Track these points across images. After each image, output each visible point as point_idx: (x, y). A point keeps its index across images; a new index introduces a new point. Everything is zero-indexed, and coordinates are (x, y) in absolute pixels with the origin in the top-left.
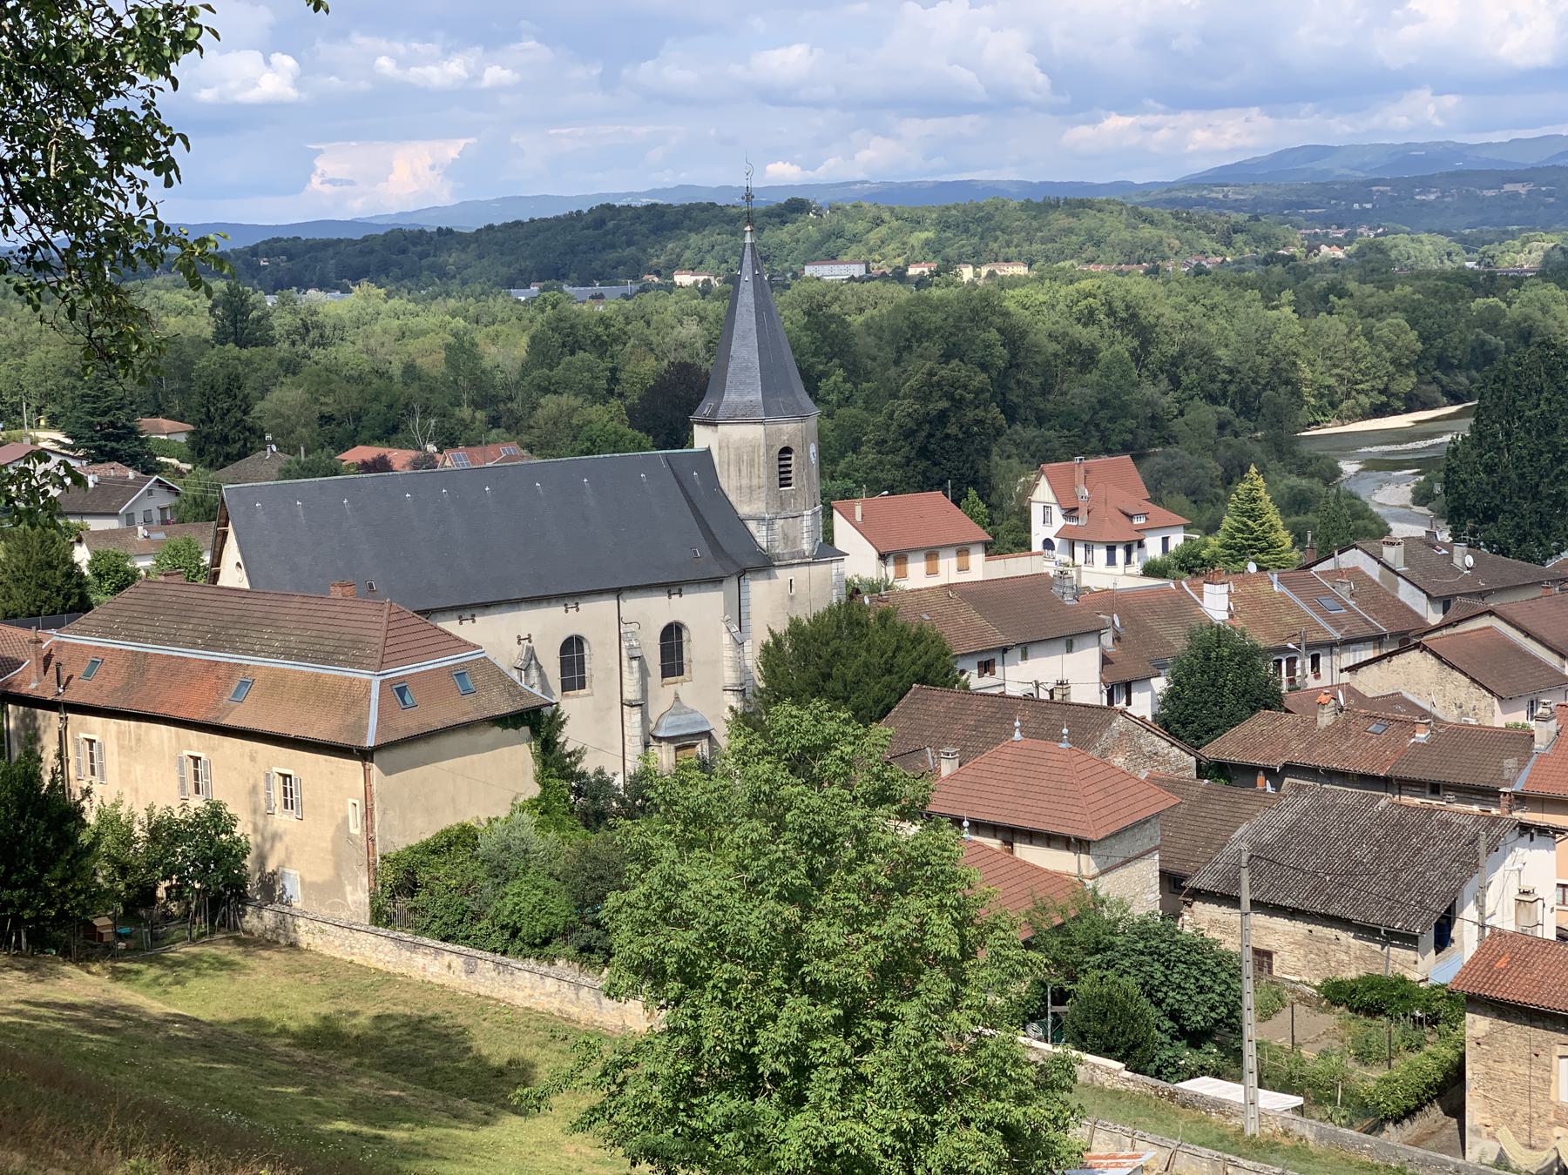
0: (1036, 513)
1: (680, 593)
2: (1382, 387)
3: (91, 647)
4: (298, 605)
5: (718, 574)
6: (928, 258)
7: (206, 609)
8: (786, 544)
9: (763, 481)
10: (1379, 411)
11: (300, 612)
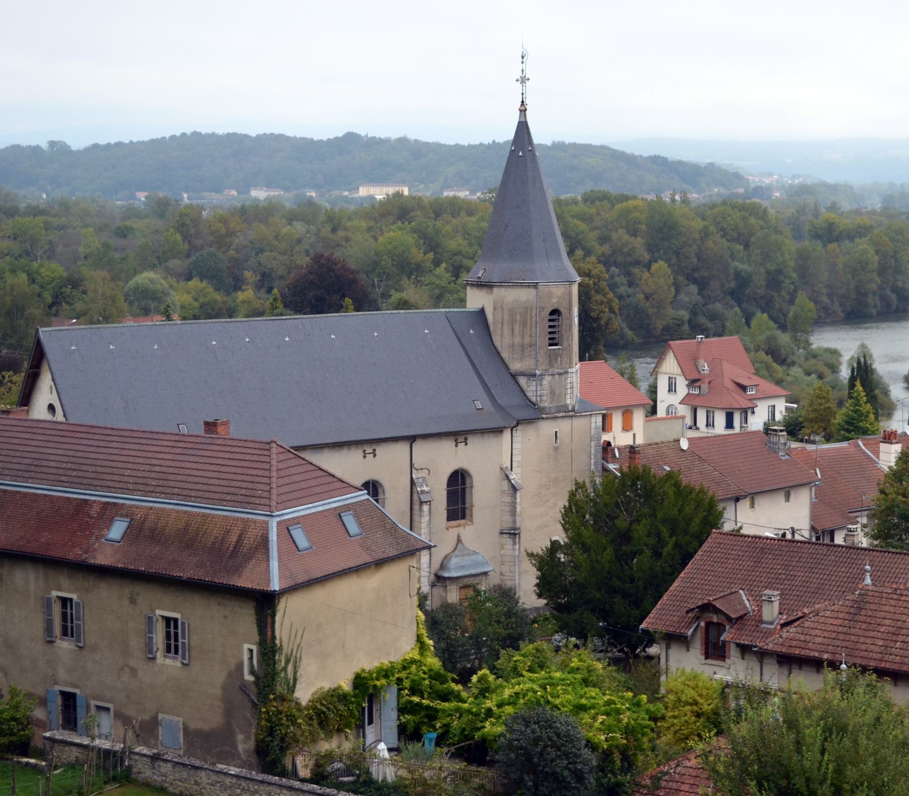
8: (552, 398)
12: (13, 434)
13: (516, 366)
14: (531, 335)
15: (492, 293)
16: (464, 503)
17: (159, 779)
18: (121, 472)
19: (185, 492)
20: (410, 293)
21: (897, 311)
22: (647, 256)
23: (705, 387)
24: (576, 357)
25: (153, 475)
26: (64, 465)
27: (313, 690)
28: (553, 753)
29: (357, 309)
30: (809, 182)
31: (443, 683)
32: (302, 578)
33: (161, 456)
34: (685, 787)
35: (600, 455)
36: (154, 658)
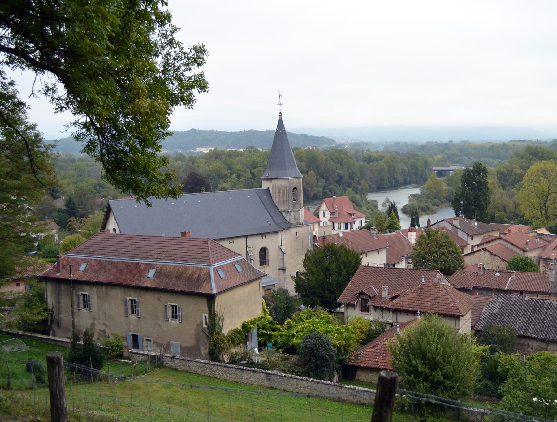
8: (295, 220)
12: (107, 239)
13: (281, 209)
16: (265, 259)
17: (174, 365)
18: (151, 252)
19: (176, 258)
20: (225, 185)
21: (395, 186)
22: (306, 169)
23: (337, 215)
24: (302, 205)
25: (163, 253)
26: (128, 250)
27: (229, 330)
28: (322, 349)
29: (206, 191)
30: (357, 142)
31: (273, 325)
32: (224, 289)
33: (166, 245)
34: (367, 359)
35: (312, 240)
36: (168, 321)
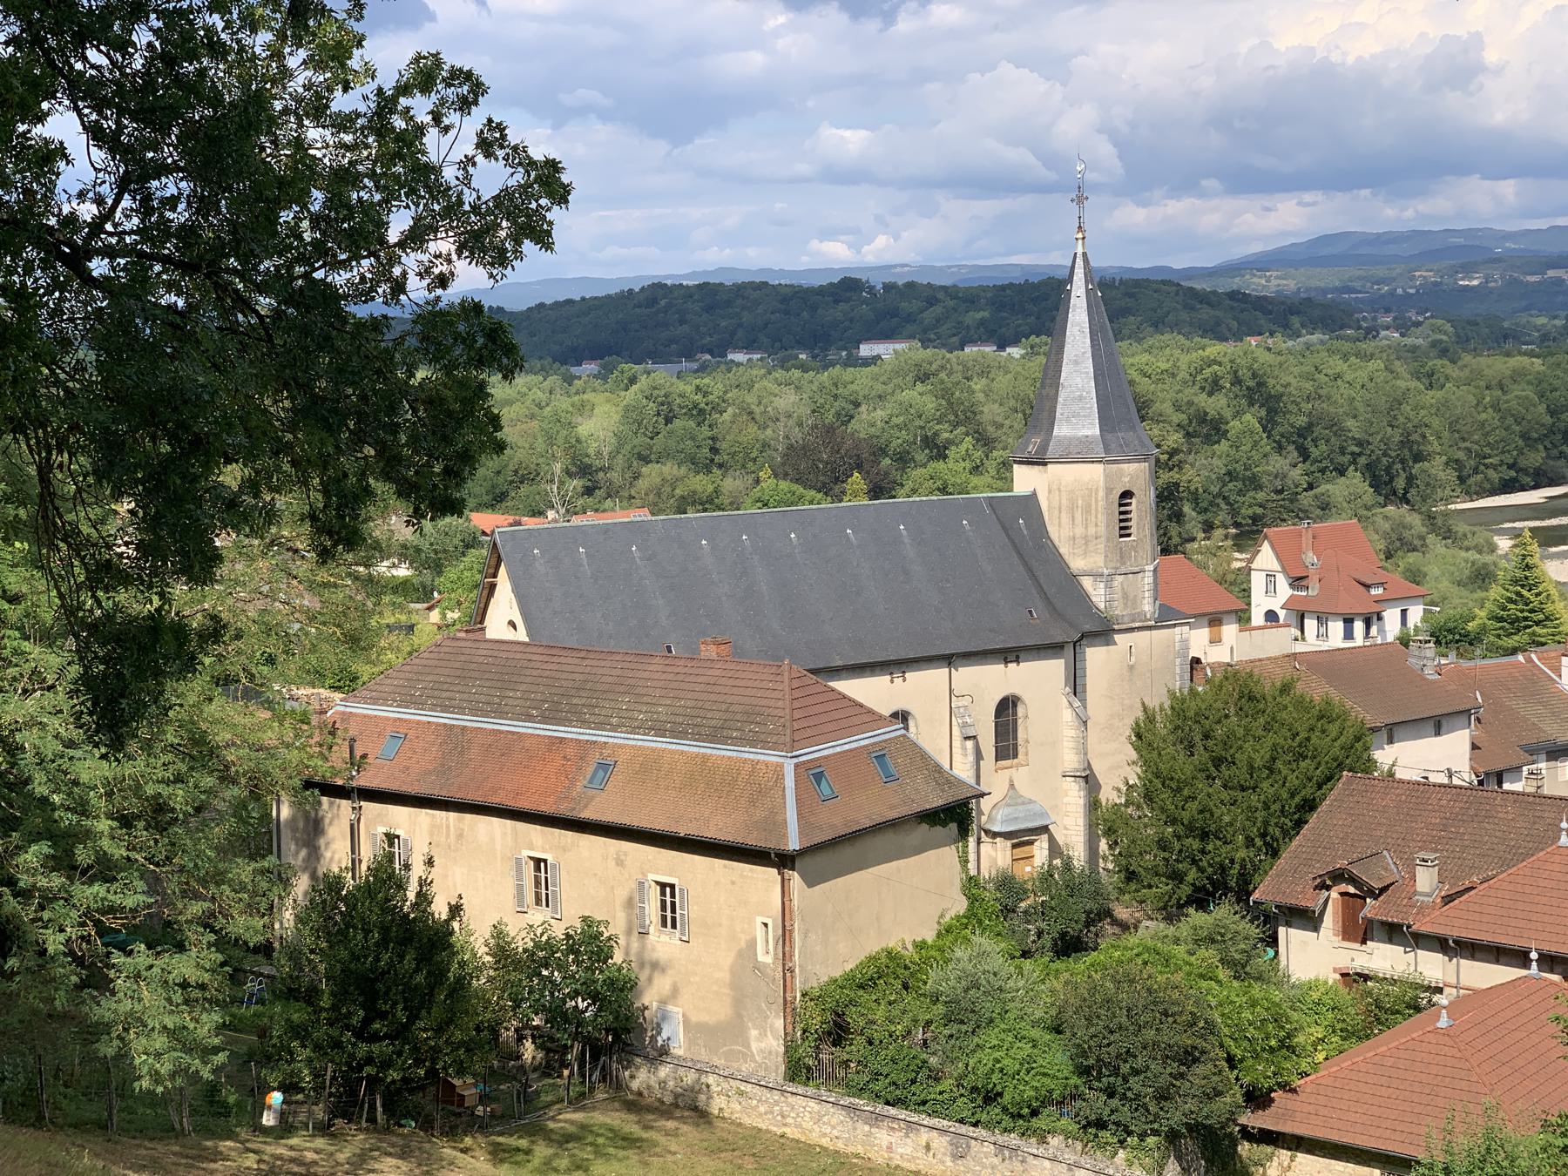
0: (1257, 582)
1: (1017, 661)
2: (1511, 461)
3: (387, 719)
4: (660, 668)
5: (1059, 639)
6: (984, 337)
7: (535, 673)
8: (1125, 604)
9: (1102, 529)
10: (1508, 487)
11: (664, 676)
14: (1096, 525)
15: (1046, 472)
